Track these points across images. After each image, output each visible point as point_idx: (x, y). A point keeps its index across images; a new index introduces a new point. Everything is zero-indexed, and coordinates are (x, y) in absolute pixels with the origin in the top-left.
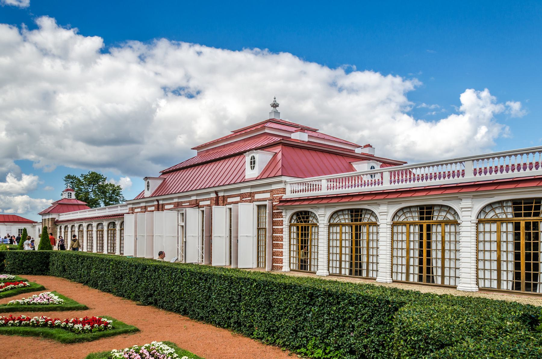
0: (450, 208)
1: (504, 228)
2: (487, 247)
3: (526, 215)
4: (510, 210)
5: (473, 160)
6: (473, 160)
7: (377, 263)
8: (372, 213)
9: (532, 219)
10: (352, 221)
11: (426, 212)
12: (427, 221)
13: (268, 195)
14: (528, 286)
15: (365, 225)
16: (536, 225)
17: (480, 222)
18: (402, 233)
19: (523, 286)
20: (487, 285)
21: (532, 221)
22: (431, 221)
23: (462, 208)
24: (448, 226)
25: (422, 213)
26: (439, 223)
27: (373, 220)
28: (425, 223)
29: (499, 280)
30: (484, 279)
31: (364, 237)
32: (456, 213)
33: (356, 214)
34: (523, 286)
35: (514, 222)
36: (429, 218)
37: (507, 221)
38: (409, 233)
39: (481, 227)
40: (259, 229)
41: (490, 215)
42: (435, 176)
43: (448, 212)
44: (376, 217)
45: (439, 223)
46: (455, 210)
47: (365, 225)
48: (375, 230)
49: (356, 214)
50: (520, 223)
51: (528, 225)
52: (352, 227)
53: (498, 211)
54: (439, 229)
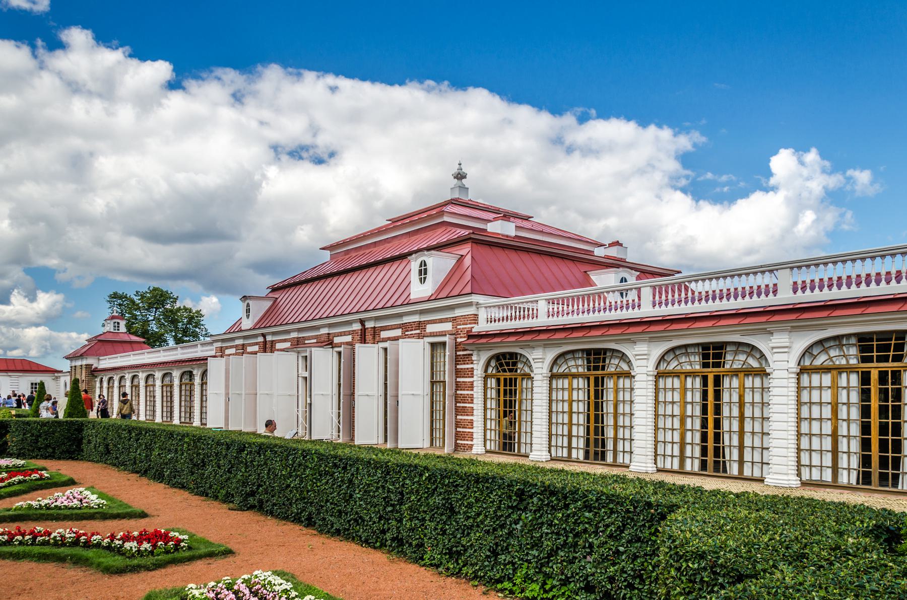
0: (753, 348)
1: (843, 380)
2: (816, 413)
3: (880, 359)
4: (853, 351)
5: (792, 268)
6: (792, 268)
7: (632, 440)
8: (623, 357)
9: (890, 366)
10: (589, 370)
11: (713, 354)
12: (715, 369)
13: (448, 327)
14: (883, 478)
15: (611, 375)
16: (897, 376)
17: (803, 370)
18: (673, 389)
19: (875, 478)
20: (816, 476)
21: (890, 370)
22: (721, 369)
23: (773, 348)
24: (751, 378)
25: (705, 356)
26: (735, 373)
27: (625, 367)
28: (711, 373)
29: (835, 468)
30: (811, 466)
31: (609, 396)
32: (763, 355)
33: (596, 358)
34: (875, 478)
35: (860, 370)
36: (717, 365)
37: (849, 369)
38: (684, 390)
39: (805, 379)
40: (433, 383)
41: (821, 360)
42: (728, 295)
43: (749, 355)
44: (629, 363)
45: (735, 373)
46: (761, 352)
47: (611, 375)
48: (627, 385)
49: (596, 358)
50: (869, 372)
51: (883, 377)
52: (588, 379)
53: (833, 353)
54: (735, 383)
